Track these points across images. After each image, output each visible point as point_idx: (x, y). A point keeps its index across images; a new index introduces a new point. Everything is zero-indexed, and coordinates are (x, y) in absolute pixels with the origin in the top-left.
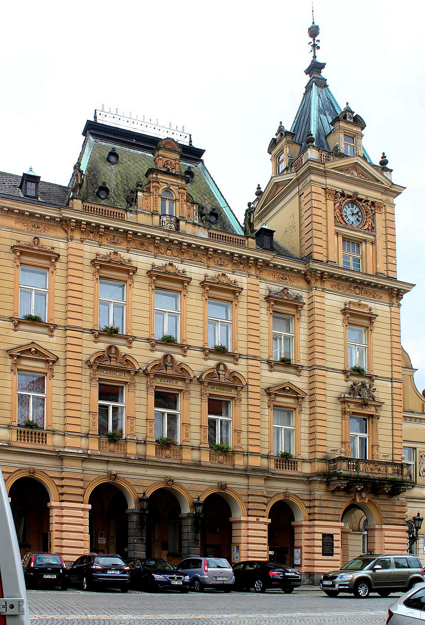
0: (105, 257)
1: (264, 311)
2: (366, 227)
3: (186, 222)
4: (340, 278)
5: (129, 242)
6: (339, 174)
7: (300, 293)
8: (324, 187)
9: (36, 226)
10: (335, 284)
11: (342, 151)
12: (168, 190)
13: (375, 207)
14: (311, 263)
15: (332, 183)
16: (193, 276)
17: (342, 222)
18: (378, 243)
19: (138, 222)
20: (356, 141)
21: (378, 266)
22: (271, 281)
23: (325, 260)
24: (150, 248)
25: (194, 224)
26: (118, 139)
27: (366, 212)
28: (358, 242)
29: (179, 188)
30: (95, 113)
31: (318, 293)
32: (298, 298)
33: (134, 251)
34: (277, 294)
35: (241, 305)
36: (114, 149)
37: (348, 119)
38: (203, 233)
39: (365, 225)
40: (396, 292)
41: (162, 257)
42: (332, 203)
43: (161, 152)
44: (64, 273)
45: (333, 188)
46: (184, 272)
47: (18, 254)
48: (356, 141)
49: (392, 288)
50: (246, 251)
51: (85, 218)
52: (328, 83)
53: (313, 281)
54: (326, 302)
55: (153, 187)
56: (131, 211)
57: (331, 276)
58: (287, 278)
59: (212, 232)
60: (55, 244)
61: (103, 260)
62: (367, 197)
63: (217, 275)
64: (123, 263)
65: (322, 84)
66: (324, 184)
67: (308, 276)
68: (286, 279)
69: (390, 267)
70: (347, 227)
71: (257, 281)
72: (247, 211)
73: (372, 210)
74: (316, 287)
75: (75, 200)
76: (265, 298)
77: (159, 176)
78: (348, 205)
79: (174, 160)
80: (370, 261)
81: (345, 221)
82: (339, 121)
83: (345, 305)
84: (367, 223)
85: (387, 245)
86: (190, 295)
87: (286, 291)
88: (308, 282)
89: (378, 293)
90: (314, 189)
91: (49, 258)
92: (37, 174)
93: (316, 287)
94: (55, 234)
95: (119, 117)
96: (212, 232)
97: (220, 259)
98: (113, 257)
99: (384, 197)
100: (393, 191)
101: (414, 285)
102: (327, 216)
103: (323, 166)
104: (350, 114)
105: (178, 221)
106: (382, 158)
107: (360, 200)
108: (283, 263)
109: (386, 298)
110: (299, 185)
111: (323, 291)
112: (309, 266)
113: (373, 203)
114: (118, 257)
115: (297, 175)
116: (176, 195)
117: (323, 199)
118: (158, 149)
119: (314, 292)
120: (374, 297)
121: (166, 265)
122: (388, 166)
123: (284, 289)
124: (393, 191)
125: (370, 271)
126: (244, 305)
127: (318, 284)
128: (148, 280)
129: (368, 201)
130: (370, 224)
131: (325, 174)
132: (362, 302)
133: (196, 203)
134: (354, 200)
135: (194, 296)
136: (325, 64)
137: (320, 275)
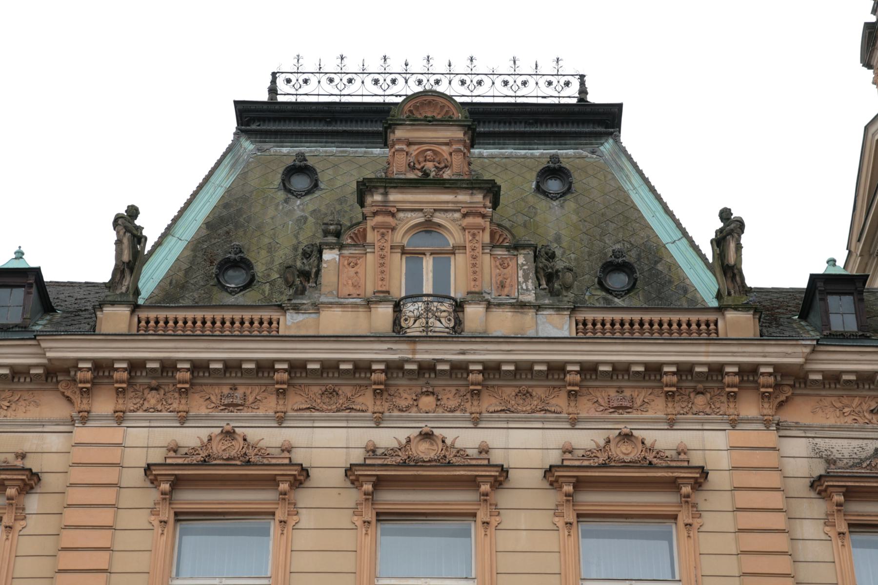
0: (589, 454)
1: (810, 529)
3: (489, 305)
5: (281, 394)
12: (429, 227)
16: (512, 460)
22: (831, 428)
24: (553, 402)
25: (521, 306)
26: (345, 131)
29: (465, 216)
30: (274, 82)
33: (301, 419)
34: (859, 464)
35: (710, 521)
36: (302, 157)
38: (556, 324)
41: (399, 419)
43: (400, 133)
44: (51, 524)
46: (484, 450)
47: (568, 488)
50: (703, 349)
51: (152, 351)
55: (373, 228)
56: (297, 308)
59: (590, 316)
60: (29, 442)
61: (586, 463)
63: (602, 443)
64: (655, 461)
71: (770, 437)
72: (743, 232)
75: (108, 310)
76: (812, 486)
77: (394, 196)
79: (446, 144)
86: (508, 519)
91: (673, 485)
92: (33, 264)
94: (33, 413)
95: (302, 77)
96: (590, 316)
97: (620, 390)
98: (218, 448)
105: (459, 306)
108: (859, 362)
114: (238, 444)
116: (454, 236)
118: (390, 127)
121: (409, 441)
126: (727, 522)
128: (551, 498)
133: (524, 247)
135: (523, 520)
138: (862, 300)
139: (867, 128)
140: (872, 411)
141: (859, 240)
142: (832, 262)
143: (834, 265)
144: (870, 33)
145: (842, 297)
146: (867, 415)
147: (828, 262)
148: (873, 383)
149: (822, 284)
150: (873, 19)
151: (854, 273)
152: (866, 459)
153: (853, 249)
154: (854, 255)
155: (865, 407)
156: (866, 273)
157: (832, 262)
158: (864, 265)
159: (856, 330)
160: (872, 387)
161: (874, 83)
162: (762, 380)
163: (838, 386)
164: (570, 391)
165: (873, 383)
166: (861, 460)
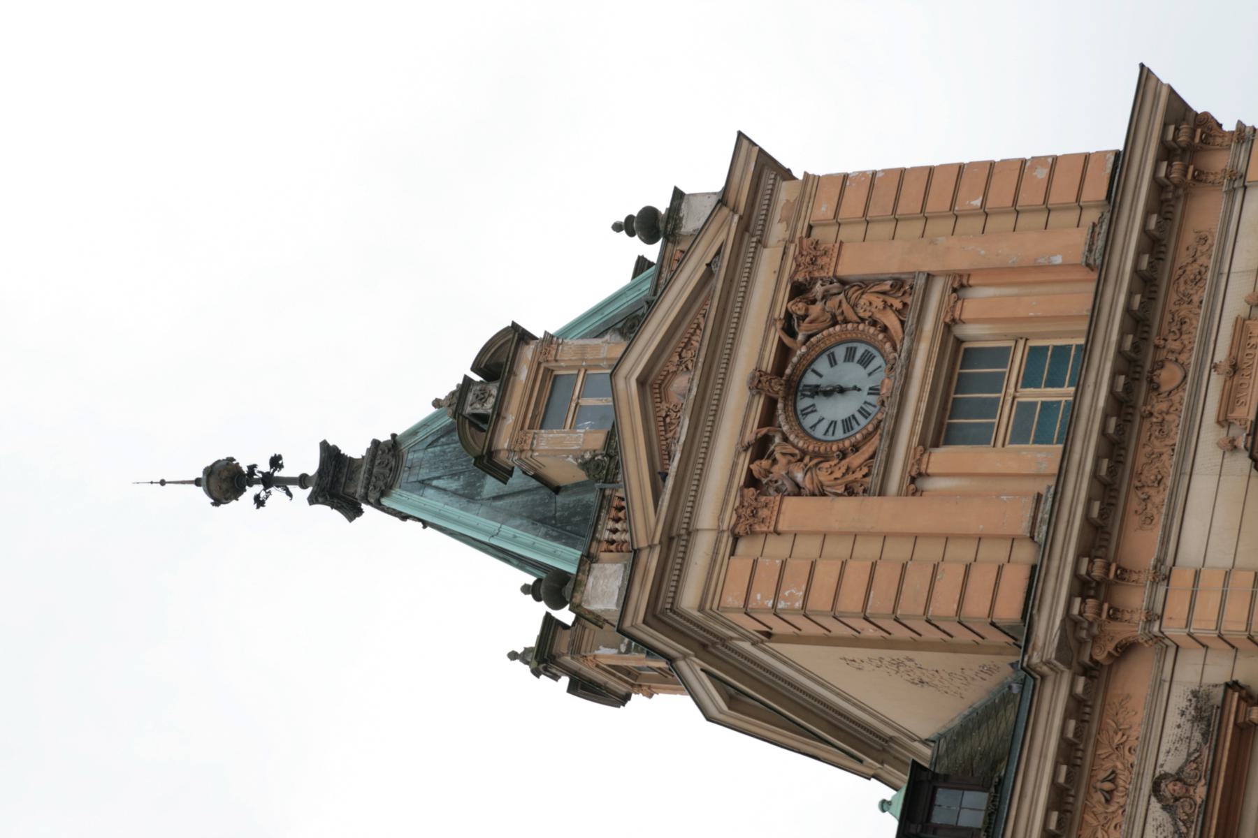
2: (891, 320)
4: (1107, 489)
6: (677, 479)
7: (1179, 700)
8: (726, 541)
9: (1108, 786)
10: (1135, 504)
11: (596, 441)
13: (813, 281)
14: (1035, 659)
15: (711, 512)
17: (867, 451)
18: (959, 262)
19: (1056, 471)
20: (567, 368)
21: (1058, 260)
23: (1025, 553)
27: (834, 324)
28: (958, 356)
31: (1177, 606)
32: (1205, 712)
37: (488, 407)
39: (885, 329)
40: (1177, 165)
42: (791, 503)
45: (734, 500)
48: (567, 368)
49: (1159, 186)
50: (1055, 563)
52: (384, 437)
53: (1121, 631)
54: (1220, 558)
57: (1098, 536)
58: (1108, 765)
62: (770, 322)
65: (388, 454)
66: (718, 542)
67: (1101, 657)
68: (1112, 777)
69: (1063, 192)
70: (888, 425)
73: (825, 297)
74: (1149, 621)
78: (805, 413)
80: (1036, 298)
81: (868, 437)
82: (491, 453)
83: (1235, 448)
84: (878, 316)
85: (971, 214)
87: (1168, 788)
88: (1126, 649)
89: (1184, 258)
90: (733, 598)
93: (1149, 621)
99: (778, 232)
100: (757, 169)
101: (1142, 66)
102: (841, 534)
103: (644, 556)
104: (470, 397)
106: (631, 234)
107: (784, 353)
108: (1033, 803)
109: (1205, 212)
110: (724, 640)
111: (1167, 578)
112: (1047, 663)
113: (799, 290)
115: (685, 657)
117: (776, 548)
119: (1173, 628)
120: (1198, 279)
122: (662, 204)
123: (1160, 799)
124: (757, 169)
125: (1078, 299)
127: (1135, 599)
129: (789, 316)
130: (878, 302)
131: (676, 539)
132: (1222, 355)
134: (784, 385)
136: (325, 446)
137: (1091, 602)
138: (946, 777)
139: (709, 718)
140: (1107, 801)
141: (861, 761)
142: (884, 805)
143: (889, 803)
144: (583, 688)
145: (937, 803)
146: (1111, 809)
147: (884, 811)
148: (1068, 790)
149: (913, 826)
150: (565, 681)
151: (907, 778)
152: (1175, 824)
153: (871, 772)
154: (880, 772)
155: (1099, 809)
156: (910, 762)
157: (884, 805)
158: (897, 762)
159: (985, 795)
160: (1072, 793)
161: (650, 696)
162: (1089, 614)
163: (1081, 747)
164: (1109, 616)
165: (1068, 790)
166: (1175, 832)
